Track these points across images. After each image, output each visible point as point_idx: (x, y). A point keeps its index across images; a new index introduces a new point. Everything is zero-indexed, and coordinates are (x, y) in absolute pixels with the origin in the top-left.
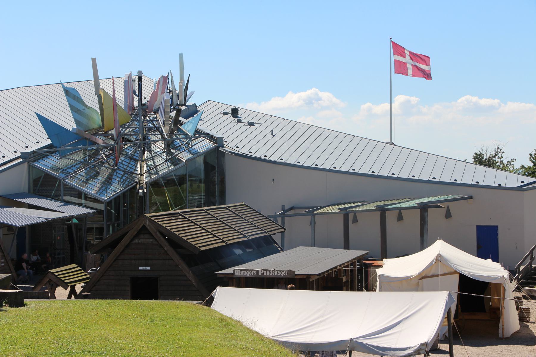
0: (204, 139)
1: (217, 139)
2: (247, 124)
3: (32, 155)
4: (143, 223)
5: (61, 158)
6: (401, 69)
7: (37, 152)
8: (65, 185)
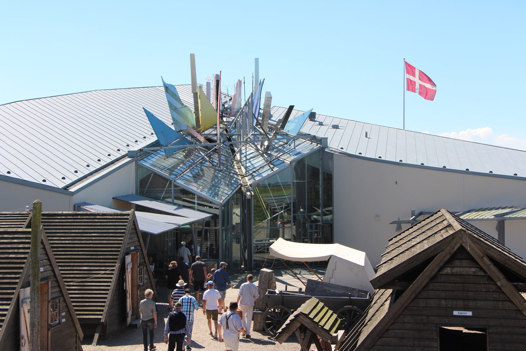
0: (305, 141)
1: (321, 139)
2: (331, 127)
3: (139, 154)
4: (461, 242)
5: (167, 157)
6: (411, 86)
7: (144, 150)
8: (176, 186)
